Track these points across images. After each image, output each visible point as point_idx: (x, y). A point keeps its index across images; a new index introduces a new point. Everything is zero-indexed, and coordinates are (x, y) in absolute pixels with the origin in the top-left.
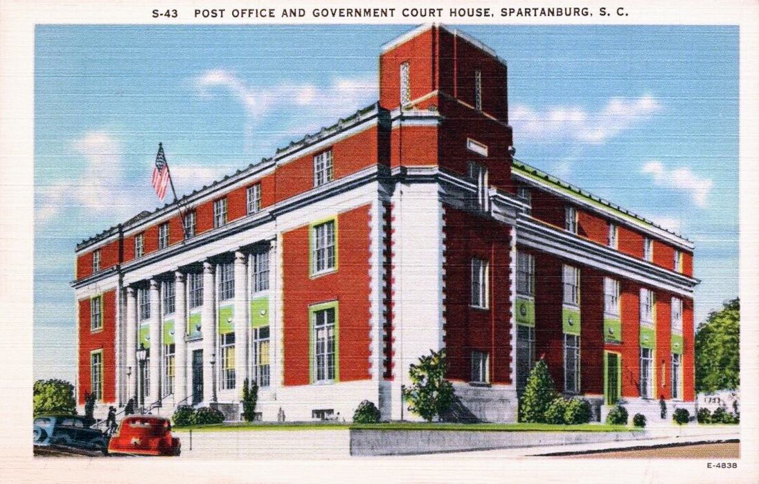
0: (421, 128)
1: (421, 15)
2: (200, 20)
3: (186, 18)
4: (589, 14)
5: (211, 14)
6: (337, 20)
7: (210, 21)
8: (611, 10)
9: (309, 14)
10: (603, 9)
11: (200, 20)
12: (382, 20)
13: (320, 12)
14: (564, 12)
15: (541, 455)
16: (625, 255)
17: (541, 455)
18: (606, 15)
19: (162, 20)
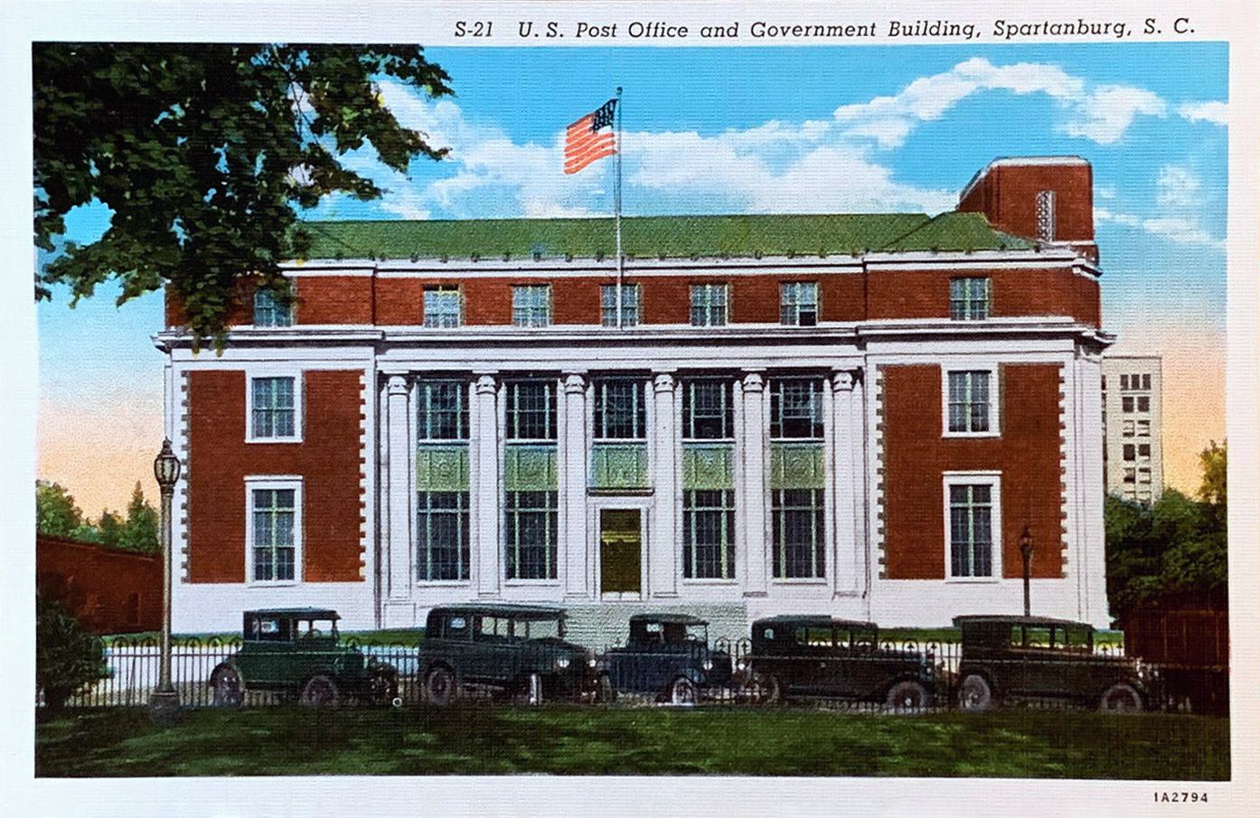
0: (320, 277)
1: (1093, 32)
2: (586, 40)
3: (504, 36)
4: (558, 34)
5: (601, 32)
6: (813, 41)
7: (600, 41)
8: (1164, 24)
9: (622, 30)
10: (552, 26)
11: (586, 40)
12: (855, 41)
13: (766, 30)
14: (901, 29)
15: (1105, 445)
16: (953, 527)
17: (1105, 445)
18: (1156, 32)
19: (468, 41)
